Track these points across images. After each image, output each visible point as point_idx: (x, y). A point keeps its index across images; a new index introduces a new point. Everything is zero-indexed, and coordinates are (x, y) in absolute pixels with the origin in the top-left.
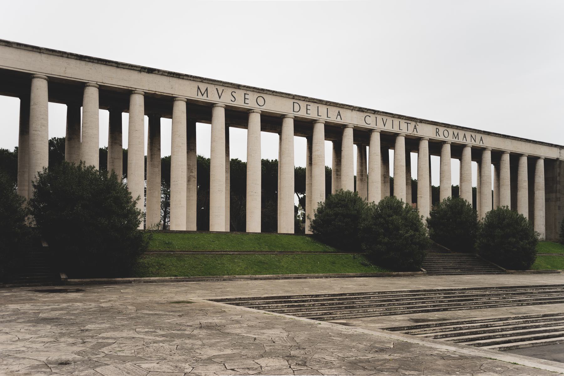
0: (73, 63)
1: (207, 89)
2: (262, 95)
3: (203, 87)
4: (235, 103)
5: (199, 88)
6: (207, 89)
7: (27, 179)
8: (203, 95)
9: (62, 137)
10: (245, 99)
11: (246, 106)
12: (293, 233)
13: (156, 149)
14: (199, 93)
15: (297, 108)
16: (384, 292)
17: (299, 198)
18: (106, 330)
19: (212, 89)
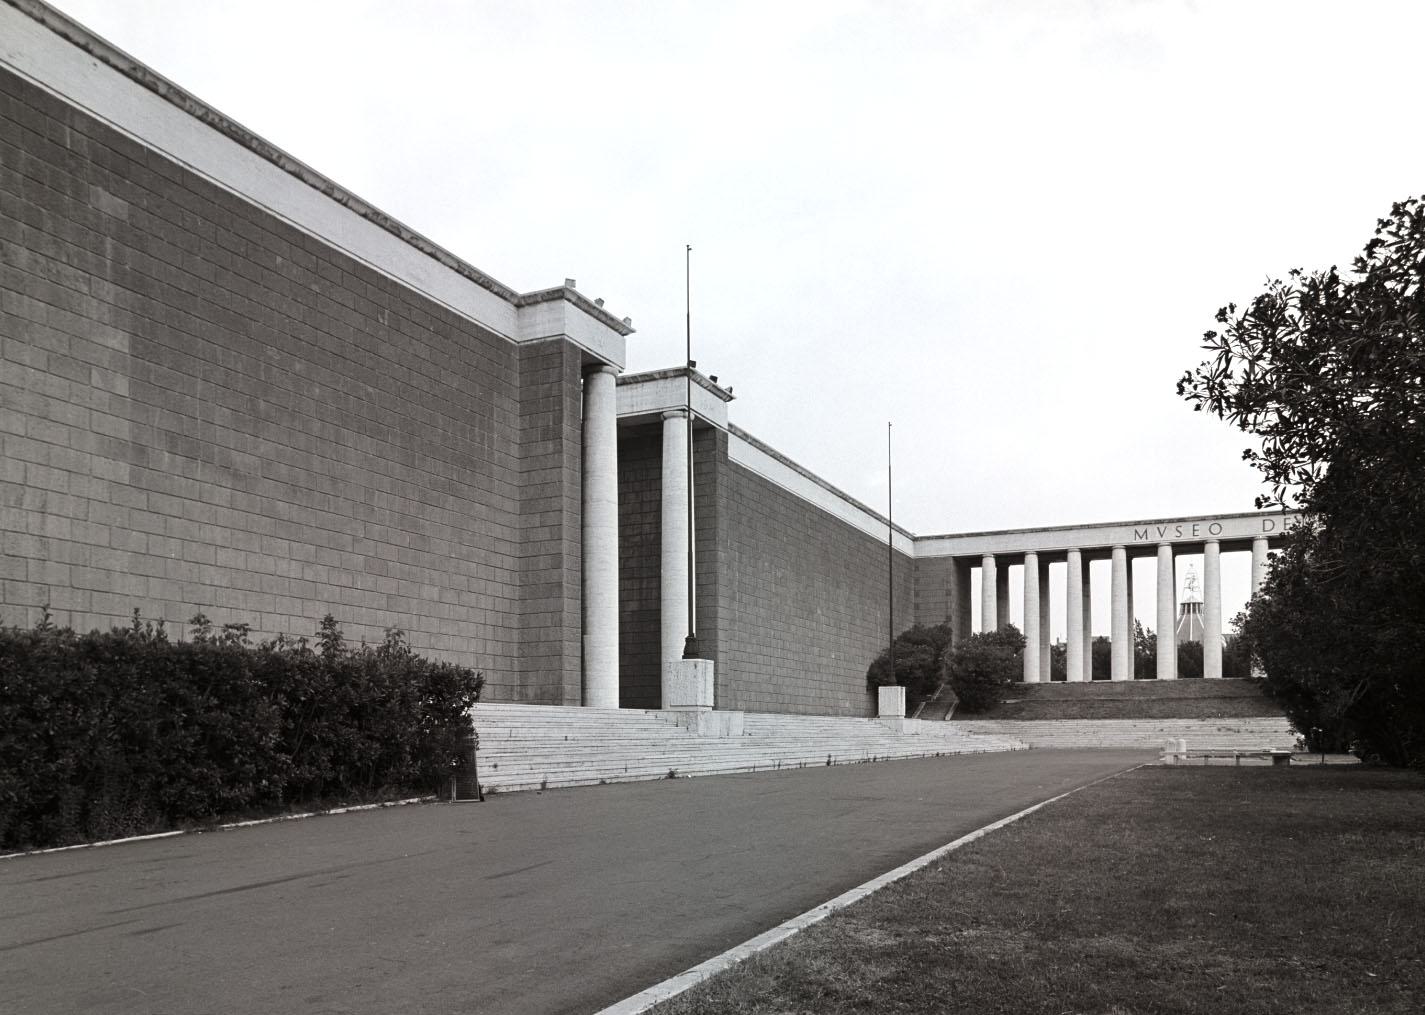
0: (1083, 533)
1: (1146, 531)
2: (1217, 522)
3: (1141, 529)
4: (1182, 538)
5: (1136, 531)
6: (1146, 531)
7: (444, 631)
8: (1141, 538)
9: (1392, 209)
10: (1194, 530)
11: (1197, 539)
12: (713, 662)
13: (605, 502)
14: (1137, 537)
15: (1269, 525)
16: (586, 311)
17: (1306, 753)
18: (1354, 340)
19: (1152, 529)
